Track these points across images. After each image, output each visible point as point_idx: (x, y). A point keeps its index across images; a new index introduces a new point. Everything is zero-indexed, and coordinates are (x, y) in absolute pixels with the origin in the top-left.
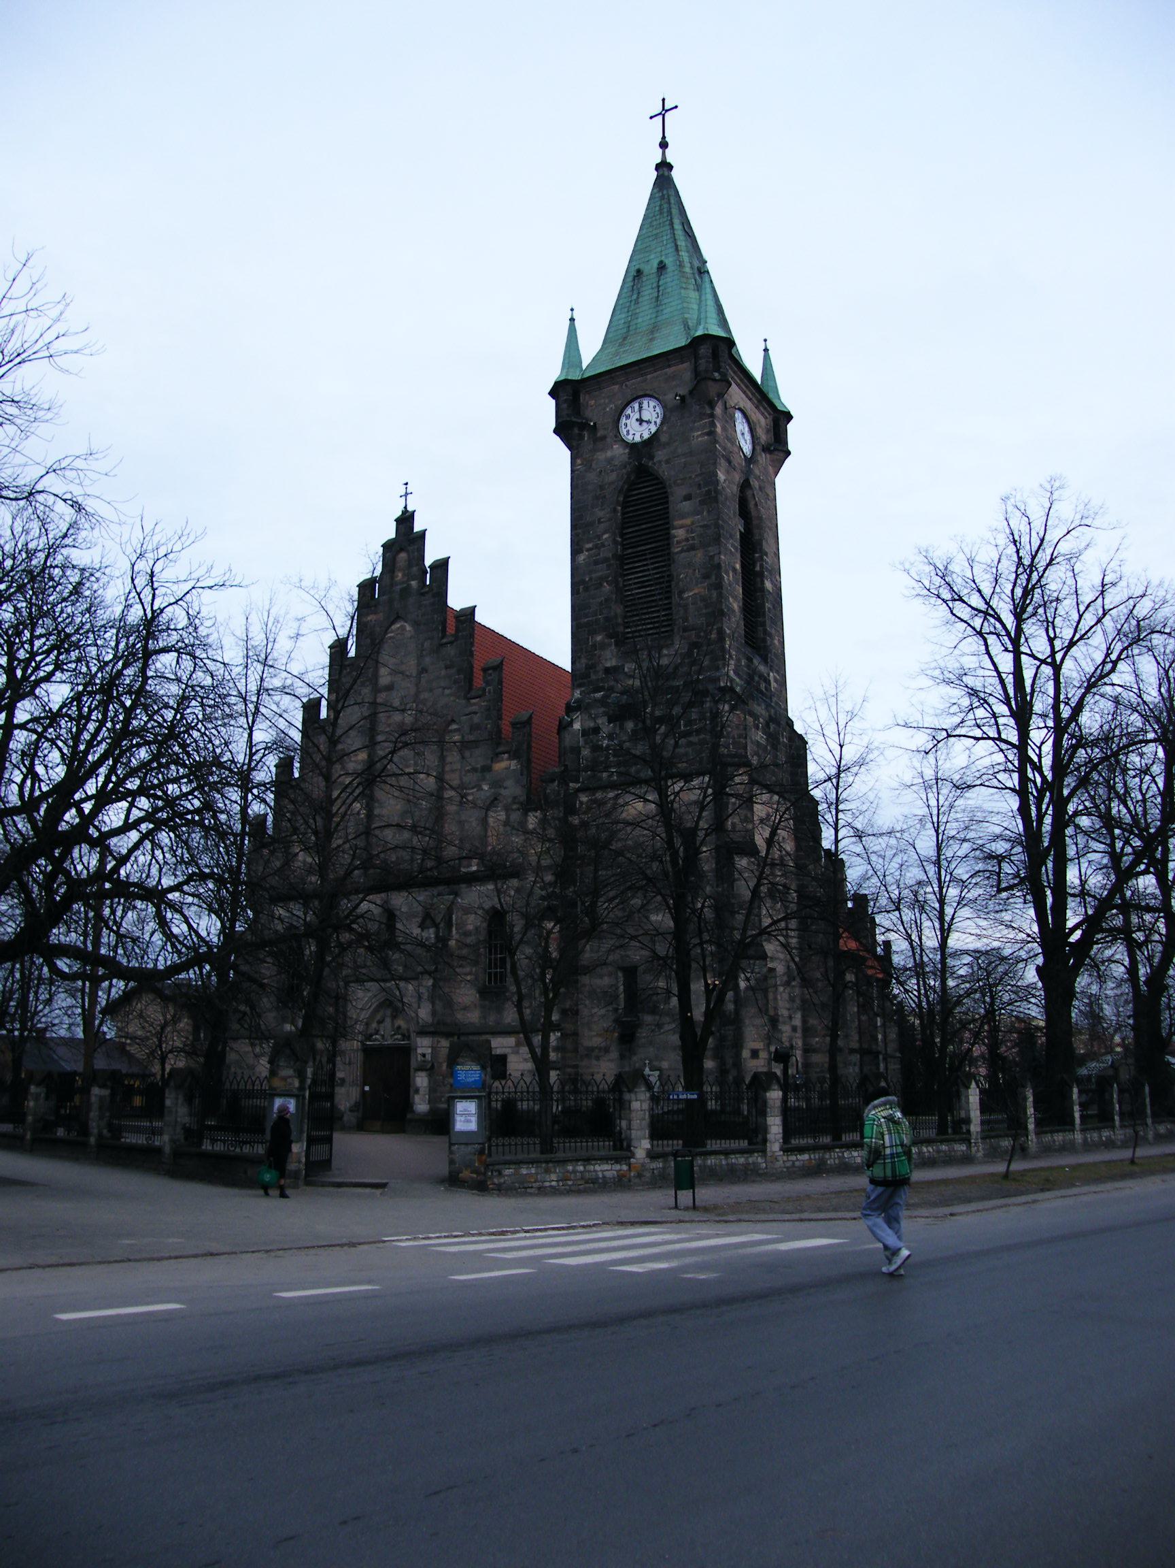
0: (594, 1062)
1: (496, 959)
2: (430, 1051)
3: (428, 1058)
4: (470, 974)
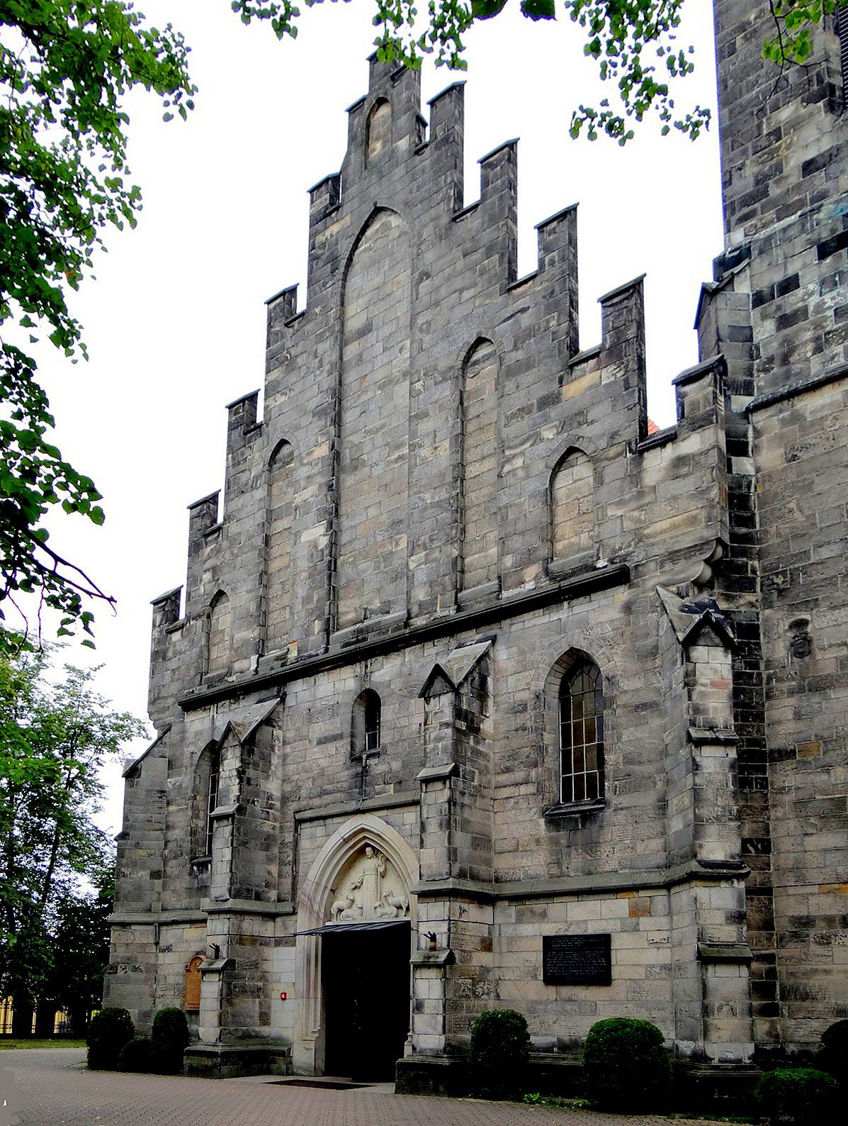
0: (814, 948)
1: (579, 779)
2: (444, 927)
3: (442, 941)
4: (526, 782)
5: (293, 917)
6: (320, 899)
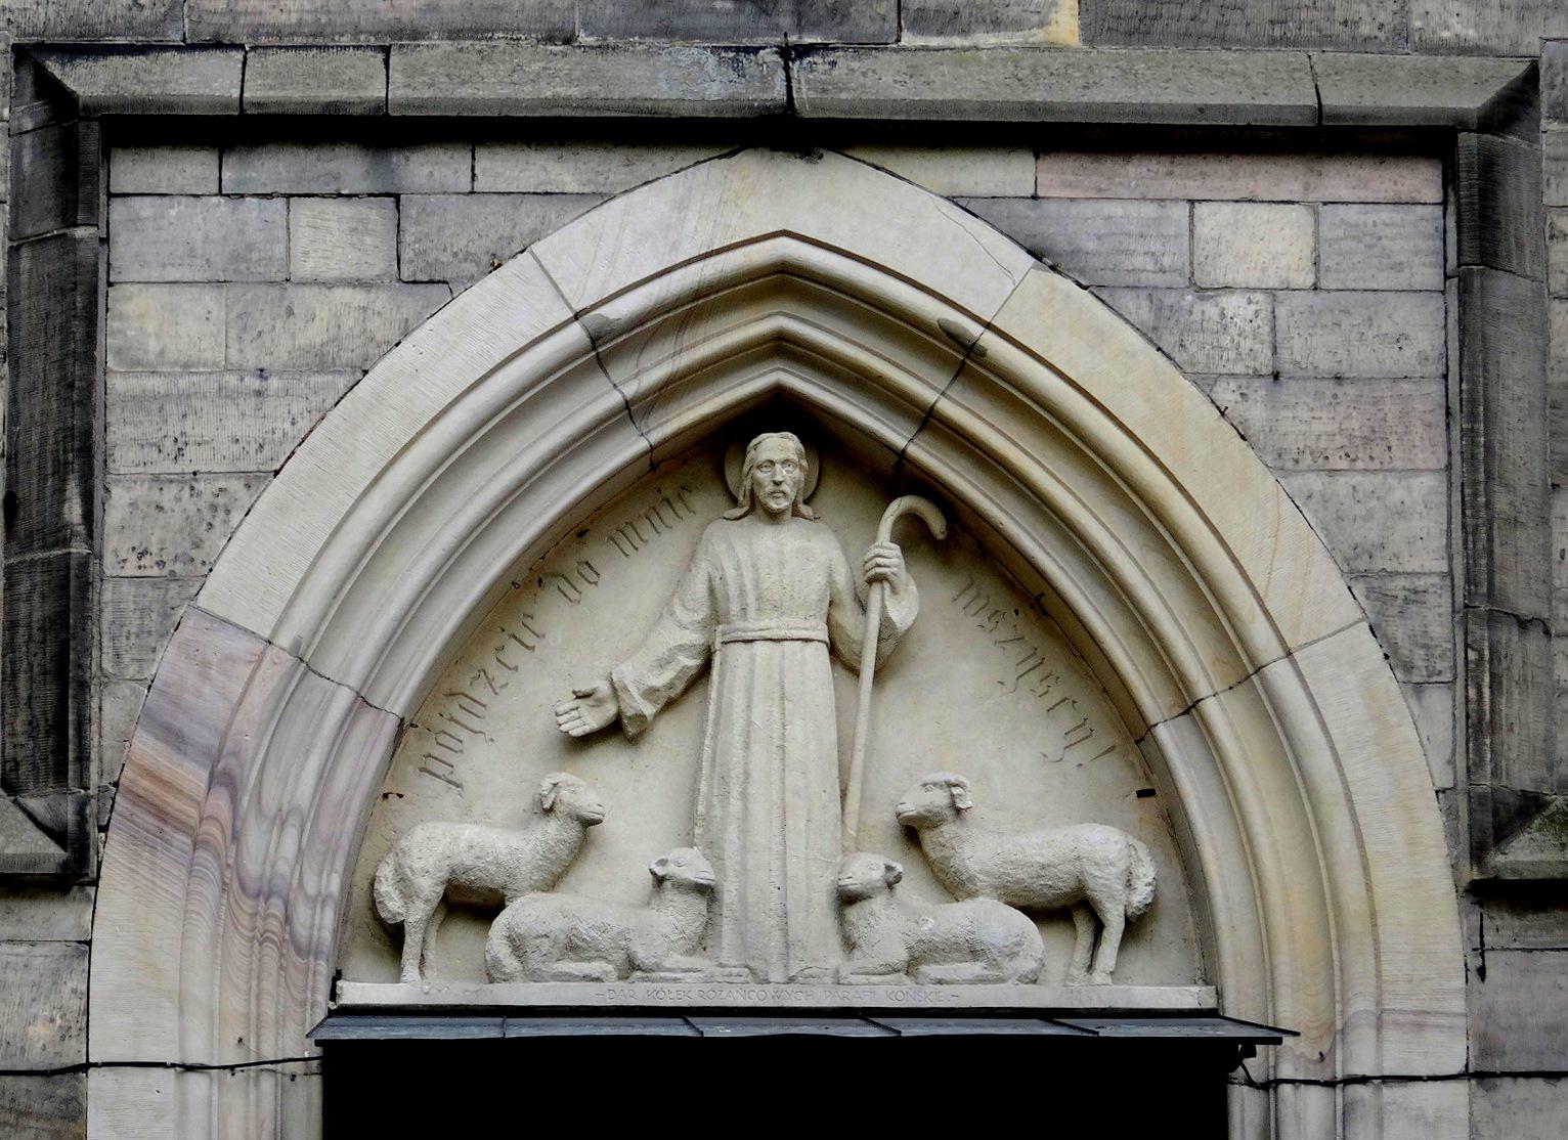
5: (61, 918)
6: (308, 774)
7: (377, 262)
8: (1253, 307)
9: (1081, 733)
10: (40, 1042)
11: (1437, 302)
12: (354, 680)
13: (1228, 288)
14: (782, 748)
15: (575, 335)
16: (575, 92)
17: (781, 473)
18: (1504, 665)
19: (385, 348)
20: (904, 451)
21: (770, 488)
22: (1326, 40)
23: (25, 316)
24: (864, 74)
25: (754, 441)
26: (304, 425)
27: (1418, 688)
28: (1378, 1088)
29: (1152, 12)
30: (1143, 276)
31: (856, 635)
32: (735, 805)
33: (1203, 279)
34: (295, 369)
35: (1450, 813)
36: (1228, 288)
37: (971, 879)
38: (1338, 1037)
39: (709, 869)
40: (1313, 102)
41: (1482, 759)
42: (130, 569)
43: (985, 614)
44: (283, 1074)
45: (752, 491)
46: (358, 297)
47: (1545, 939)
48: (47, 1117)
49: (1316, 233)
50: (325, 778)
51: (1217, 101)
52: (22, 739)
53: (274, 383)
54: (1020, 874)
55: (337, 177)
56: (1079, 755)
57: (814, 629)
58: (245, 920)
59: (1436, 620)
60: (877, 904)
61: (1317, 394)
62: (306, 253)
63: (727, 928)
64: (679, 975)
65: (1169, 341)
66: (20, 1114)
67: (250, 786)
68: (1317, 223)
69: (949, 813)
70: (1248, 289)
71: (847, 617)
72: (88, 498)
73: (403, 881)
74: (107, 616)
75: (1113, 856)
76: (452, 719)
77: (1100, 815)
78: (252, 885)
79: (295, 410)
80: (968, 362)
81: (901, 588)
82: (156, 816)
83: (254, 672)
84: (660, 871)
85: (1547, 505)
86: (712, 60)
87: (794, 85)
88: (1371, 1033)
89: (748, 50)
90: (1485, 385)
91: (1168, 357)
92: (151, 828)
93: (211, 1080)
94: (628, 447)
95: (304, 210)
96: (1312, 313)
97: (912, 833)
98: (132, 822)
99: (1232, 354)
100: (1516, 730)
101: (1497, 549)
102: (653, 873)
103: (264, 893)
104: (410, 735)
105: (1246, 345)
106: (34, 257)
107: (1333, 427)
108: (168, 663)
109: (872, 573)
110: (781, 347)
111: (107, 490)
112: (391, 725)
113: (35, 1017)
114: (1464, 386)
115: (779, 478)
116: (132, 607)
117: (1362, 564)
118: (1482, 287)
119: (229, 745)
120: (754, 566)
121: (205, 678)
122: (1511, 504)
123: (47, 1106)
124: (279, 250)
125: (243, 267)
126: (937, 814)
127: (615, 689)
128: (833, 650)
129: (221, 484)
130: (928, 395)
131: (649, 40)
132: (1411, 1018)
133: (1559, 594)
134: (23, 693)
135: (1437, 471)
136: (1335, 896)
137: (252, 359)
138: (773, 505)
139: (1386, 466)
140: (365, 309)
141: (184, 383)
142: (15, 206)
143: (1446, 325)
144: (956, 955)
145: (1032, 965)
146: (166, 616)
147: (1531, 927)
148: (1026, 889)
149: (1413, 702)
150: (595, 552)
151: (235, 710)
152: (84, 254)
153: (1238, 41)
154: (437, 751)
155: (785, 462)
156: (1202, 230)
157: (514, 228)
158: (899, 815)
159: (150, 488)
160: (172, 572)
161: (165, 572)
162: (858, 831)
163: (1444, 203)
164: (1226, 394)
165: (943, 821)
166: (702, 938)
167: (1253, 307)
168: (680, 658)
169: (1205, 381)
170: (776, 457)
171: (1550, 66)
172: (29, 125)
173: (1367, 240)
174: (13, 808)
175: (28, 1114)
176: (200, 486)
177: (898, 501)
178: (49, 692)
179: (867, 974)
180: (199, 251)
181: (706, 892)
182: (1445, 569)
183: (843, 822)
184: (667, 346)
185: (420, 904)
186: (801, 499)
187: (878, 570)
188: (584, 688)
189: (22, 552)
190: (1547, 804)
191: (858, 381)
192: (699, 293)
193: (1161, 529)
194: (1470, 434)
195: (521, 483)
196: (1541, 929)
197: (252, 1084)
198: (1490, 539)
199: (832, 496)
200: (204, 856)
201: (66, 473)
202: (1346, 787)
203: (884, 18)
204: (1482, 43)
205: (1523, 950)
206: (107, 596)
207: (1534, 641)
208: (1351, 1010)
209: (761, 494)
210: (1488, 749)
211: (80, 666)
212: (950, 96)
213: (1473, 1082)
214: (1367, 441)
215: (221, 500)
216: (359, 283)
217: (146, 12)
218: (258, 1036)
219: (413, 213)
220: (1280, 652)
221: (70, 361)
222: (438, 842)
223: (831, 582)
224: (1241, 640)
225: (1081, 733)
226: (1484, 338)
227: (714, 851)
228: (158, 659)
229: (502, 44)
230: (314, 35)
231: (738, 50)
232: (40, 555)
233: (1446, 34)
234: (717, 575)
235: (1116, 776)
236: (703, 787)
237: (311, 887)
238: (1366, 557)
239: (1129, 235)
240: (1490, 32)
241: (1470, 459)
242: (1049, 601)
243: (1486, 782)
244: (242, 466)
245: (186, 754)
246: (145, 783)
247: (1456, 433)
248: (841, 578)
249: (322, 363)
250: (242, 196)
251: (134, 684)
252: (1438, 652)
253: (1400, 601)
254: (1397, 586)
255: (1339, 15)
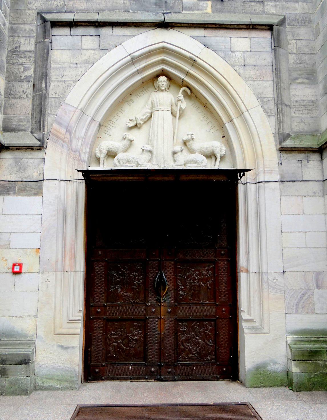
5: (39, 154)
6: (84, 131)
7: (96, 46)
8: (241, 54)
9: (213, 127)
10: (35, 176)
11: (270, 54)
12: (91, 115)
13: (236, 51)
14: (163, 128)
15: (129, 58)
16: (129, 18)
17: (163, 83)
18: (284, 112)
19: (97, 60)
20: (183, 79)
21: (161, 85)
22: (251, 13)
23: (37, 55)
24: (177, 16)
25: (159, 78)
26: (83, 72)
27: (269, 116)
28: (264, 184)
29: (223, 8)
30: (222, 49)
31: (176, 110)
32: (156, 137)
33: (232, 50)
34: (82, 63)
35: (275, 137)
36: (236, 51)
37: (195, 150)
38: (257, 175)
39: (151, 148)
40: (250, 20)
41: (280, 127)
42: (54, 96)
43: (197, 107)
44: (78, 182)
45: (159, 87)
46: (93, 52)
47: (291, 158)
48: (36, 189)
49: (250, 43)
50: (86, 132)
51: (234, 20)
52: (34, 124)
53: (79, 66)
54: (203, 149)
55: (90, 32)
56: (212, 131)
57: (169, 109)
58: (72, 156)
59: (272, 105)
60: (179, 154)
61: (252, 68)
62: (84, 45)
63: (154, 158)
64: (146, 166)
65: (227, 60)
66: (32, 188)
67: (73, 133)
68: (251, 41)
69: (191, 139)
70: (240, 51)
71: (174, 108)
72: (46, 83)
73: (100, 151)
74: (49, 104)
75: (219, 147)
76: (109, 125)
77: (216, 140)
78: (74, 150)
79: (82, 70)
80: (194, 63)
81: (183, 103)
82: (57, 137)
83: (74, 113)
84: (143, 148)
85: (289, 87)
86: (152, 14)
87: (165, 17)
88: (263, 174)
89: (157, 13)
90: (279, 66)
91: (227, 62)
92: (56, 139)
93: (65, 183)
94: (138, 78)
95: (84, 38)
96: (250, 55)
97: (185, 143)
98: (52, 138)
99: (237, 62)
100: (286, 122)
101: (282, 93)
102: (142, 149)
103: (75, 151)
104: (102, 127)
105: (240, 60)
106: (39, 45)
107: (254, 74)
108: (59, 112)
109: (178, 99)
110: (163, 62)
111: (50, 83)
112: (98, 124)
113: (35, 171)
114: (276, 66)
115: (163, 84)
116: (54, 102)
117: (259, 96)
118: (278, 50)
119: (69, 125)
120: (159, 98)
121: (66, 114)
122: (284, 86)
123: (36, 187)
124: (80, 44)
125: (74, 47)
126: (189, 139)
127: (136, 119)
128: (172, 113)
129: (69, 82)
130: (187, 69)
131: (142, 12)
132: (270, 171)
133: (292, 101)
134: (35, 117)
135: (271, 81)
136: (256, 151)
137: (75, 62)
138: (162, 88)
139: (263, 80)
140: (94, 54)
141: (63, 66)
142: (36, 37)
143: (272, 57)
144: (192, 163)
145: (205, 164)
146: (59, 104)
147: (289, 156)
148: (204, 152)
149: (268, 118)
150: (133, 97)
151: (71, 120)
152: (47, 43)
153: (237, 13)
154: (107, 130)
155: (164, 81)
156: (232, 42)
157: (119, 40)
158: (183, 140)
159: (57, 83)
160: (61, 97)
161: (59, 96)
162: (176, 143)
163: (271, 38)
164: (236, 68)
165: (190, 141)
166: (150, 160)
167: (241, 54)
168: (147, 114)
169: (233, 66)
170: (162, 80)
171: (287, 17)
172: (39, 24)
173: (259, 44)
174: (32, 136)
175: (33, 188)
176: (66, 82)
177: (182, 88)
178: (39, 116)
179: (178, 165)
180: (67, 44)
181: (151, 152)
182: (273, 97)
183: (174, 141)
184: (144, 61)
185: (103, 154)
186: (167, 88)
187: (180, 99)
188: (131, 119)
189: (35, 93)
190: (291, 136)
191: (176, 67)
192: (149, 52)
193: (226, 91)
194: (277, 74)
195: (120, 83)
196: (291, 156)
197: (72, 184)
198: (281, 91)
199: (172, 88)
200: (64, 144)
201: (43, 79)
202: (258, 133)
203: (180, 8)
204: (276, 13)
205: (288, 160)
206: (50, 100)
207: (288, 108)
208: (259, 171)
209: (160, 87)
210: (282, 125)
211: (44, 111)
212: (191, 19)
213: (280, 182)
214: (260, 76)
215: (69, 85)
216: (93, 49)
217: (59, 7)
218: (74, 175)
219: (102, 38)
220: (246, 110)
221: (44, 61)
222: (106, 144)
223: (172, 102)
224: (239, 136)
225: (213, 127)
226: (279, 58)
227: (152, 145)
228: (58, 111)
229: (117, 12)
230: (87, 11)
231: (156, 13)
232: (38, 93)
233: (270, 12)
234: (153, 100)
235: (219, 134)
236: (150, 135)
237: (84, 151)
238: (260, 95)
239: (220, 43)
240: (277, 12)
241: (277, 78)
242: (208, 105)
243: (281, 131)
244: (73, 79)
245: (62, 127)
246: (55, 132)
247: (274, 74)
248: (173, 101)
249: (87, 62)
250: (74, 36)
251: (54, 115)
252: (272, 110)
253: (266, 102)
254: (265, 99)
255: (253, 9)
